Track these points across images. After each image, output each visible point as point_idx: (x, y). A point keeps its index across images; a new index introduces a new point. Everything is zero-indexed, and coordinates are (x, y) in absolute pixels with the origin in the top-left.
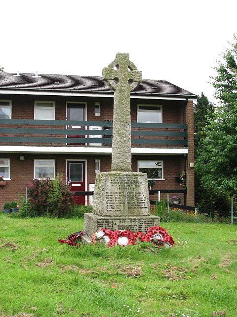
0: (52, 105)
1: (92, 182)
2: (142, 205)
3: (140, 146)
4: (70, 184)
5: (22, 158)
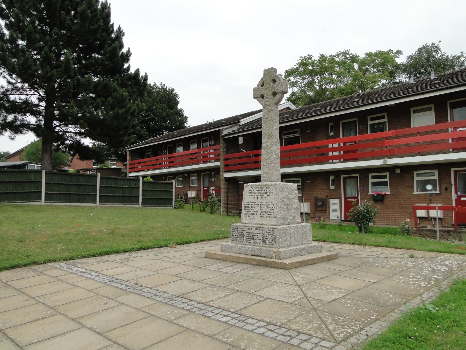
0: (430, 109)
1: (101, 201)
2: (272, 215)
3: (290, 165)
4: (459, 197)
5: (398, 171)
